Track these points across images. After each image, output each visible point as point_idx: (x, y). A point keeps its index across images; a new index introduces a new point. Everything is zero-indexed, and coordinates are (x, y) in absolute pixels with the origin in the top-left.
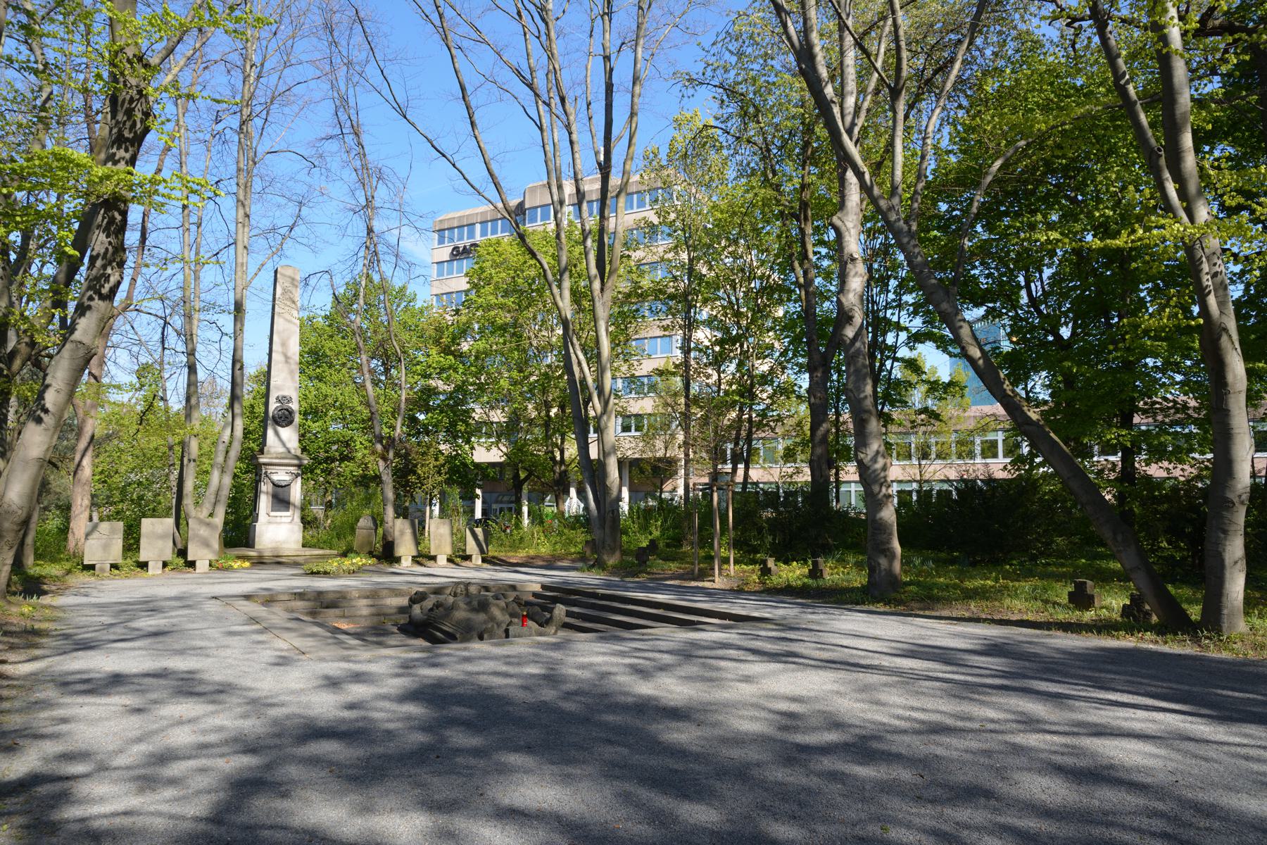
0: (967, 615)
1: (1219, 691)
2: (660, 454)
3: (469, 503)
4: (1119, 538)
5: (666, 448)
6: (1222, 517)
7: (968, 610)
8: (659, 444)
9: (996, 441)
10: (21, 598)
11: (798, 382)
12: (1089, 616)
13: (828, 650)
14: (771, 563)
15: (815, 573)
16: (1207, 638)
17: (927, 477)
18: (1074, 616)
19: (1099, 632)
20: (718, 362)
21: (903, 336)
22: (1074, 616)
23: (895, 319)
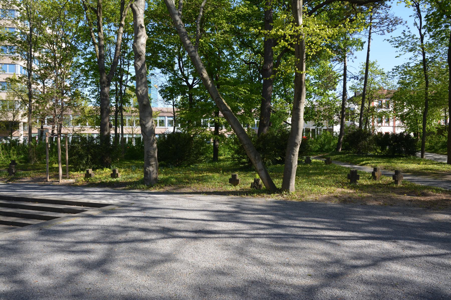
0: (191, 191)
1: (384, 229)
2: (11, 119)
3: (146, 178)
4: (257, 158)
5: (14, 116)
6: (293, 149)
7: (191, 189)
8: (10, 114)
9: (306, 120)
10: (146, 9)
11: (83, 91)
12: (238, 188)
13: (181, 223)
14: (91, 171)
15: (114, 175)
16: (285, 194)
17: (135, 132)
18: (231, 188)
19: (247, 195)
20: (43, 78)
21: (129, 77)
22: (231, 188)
23: (126, 69)
